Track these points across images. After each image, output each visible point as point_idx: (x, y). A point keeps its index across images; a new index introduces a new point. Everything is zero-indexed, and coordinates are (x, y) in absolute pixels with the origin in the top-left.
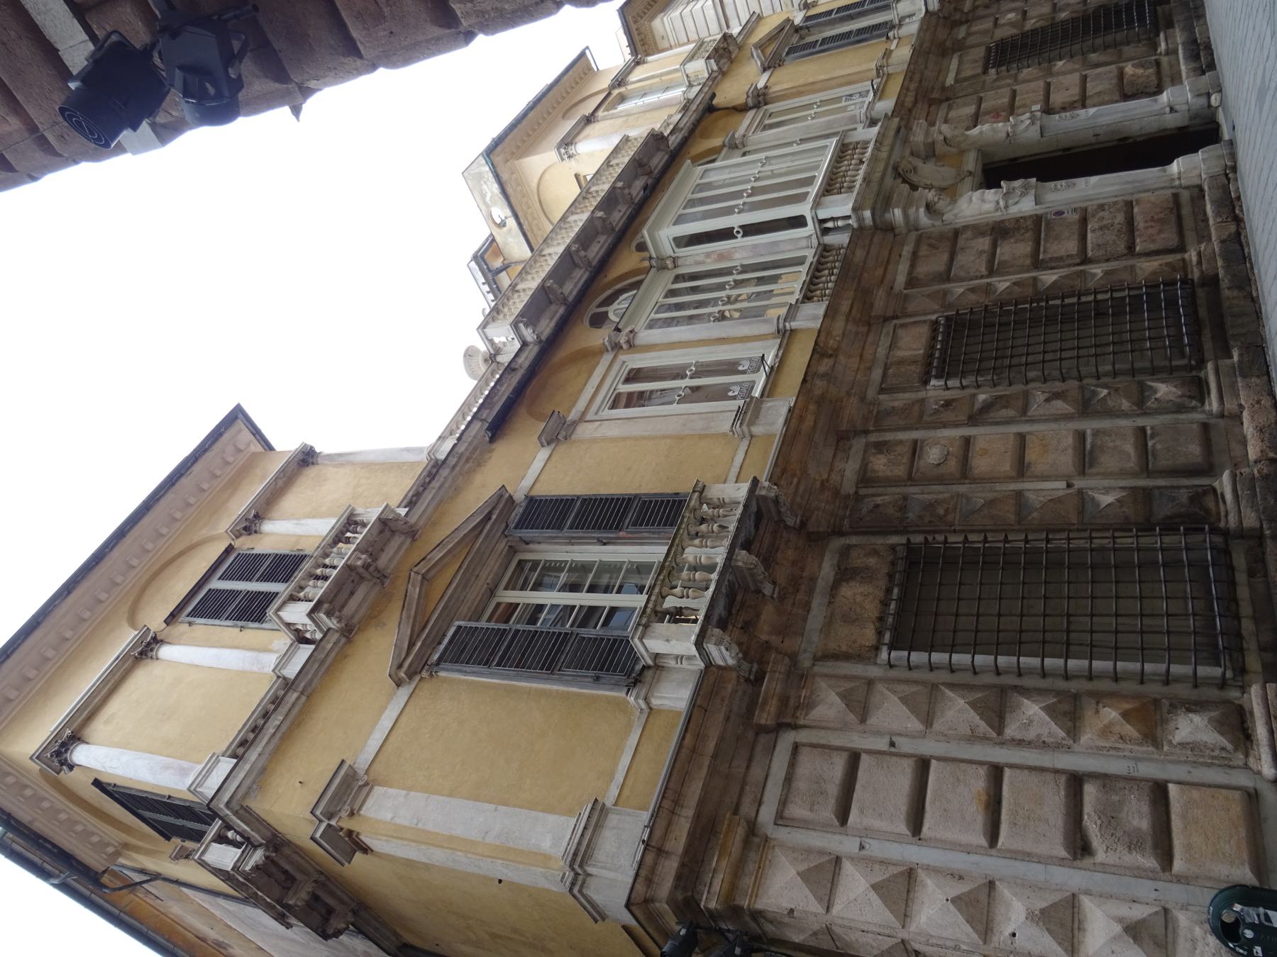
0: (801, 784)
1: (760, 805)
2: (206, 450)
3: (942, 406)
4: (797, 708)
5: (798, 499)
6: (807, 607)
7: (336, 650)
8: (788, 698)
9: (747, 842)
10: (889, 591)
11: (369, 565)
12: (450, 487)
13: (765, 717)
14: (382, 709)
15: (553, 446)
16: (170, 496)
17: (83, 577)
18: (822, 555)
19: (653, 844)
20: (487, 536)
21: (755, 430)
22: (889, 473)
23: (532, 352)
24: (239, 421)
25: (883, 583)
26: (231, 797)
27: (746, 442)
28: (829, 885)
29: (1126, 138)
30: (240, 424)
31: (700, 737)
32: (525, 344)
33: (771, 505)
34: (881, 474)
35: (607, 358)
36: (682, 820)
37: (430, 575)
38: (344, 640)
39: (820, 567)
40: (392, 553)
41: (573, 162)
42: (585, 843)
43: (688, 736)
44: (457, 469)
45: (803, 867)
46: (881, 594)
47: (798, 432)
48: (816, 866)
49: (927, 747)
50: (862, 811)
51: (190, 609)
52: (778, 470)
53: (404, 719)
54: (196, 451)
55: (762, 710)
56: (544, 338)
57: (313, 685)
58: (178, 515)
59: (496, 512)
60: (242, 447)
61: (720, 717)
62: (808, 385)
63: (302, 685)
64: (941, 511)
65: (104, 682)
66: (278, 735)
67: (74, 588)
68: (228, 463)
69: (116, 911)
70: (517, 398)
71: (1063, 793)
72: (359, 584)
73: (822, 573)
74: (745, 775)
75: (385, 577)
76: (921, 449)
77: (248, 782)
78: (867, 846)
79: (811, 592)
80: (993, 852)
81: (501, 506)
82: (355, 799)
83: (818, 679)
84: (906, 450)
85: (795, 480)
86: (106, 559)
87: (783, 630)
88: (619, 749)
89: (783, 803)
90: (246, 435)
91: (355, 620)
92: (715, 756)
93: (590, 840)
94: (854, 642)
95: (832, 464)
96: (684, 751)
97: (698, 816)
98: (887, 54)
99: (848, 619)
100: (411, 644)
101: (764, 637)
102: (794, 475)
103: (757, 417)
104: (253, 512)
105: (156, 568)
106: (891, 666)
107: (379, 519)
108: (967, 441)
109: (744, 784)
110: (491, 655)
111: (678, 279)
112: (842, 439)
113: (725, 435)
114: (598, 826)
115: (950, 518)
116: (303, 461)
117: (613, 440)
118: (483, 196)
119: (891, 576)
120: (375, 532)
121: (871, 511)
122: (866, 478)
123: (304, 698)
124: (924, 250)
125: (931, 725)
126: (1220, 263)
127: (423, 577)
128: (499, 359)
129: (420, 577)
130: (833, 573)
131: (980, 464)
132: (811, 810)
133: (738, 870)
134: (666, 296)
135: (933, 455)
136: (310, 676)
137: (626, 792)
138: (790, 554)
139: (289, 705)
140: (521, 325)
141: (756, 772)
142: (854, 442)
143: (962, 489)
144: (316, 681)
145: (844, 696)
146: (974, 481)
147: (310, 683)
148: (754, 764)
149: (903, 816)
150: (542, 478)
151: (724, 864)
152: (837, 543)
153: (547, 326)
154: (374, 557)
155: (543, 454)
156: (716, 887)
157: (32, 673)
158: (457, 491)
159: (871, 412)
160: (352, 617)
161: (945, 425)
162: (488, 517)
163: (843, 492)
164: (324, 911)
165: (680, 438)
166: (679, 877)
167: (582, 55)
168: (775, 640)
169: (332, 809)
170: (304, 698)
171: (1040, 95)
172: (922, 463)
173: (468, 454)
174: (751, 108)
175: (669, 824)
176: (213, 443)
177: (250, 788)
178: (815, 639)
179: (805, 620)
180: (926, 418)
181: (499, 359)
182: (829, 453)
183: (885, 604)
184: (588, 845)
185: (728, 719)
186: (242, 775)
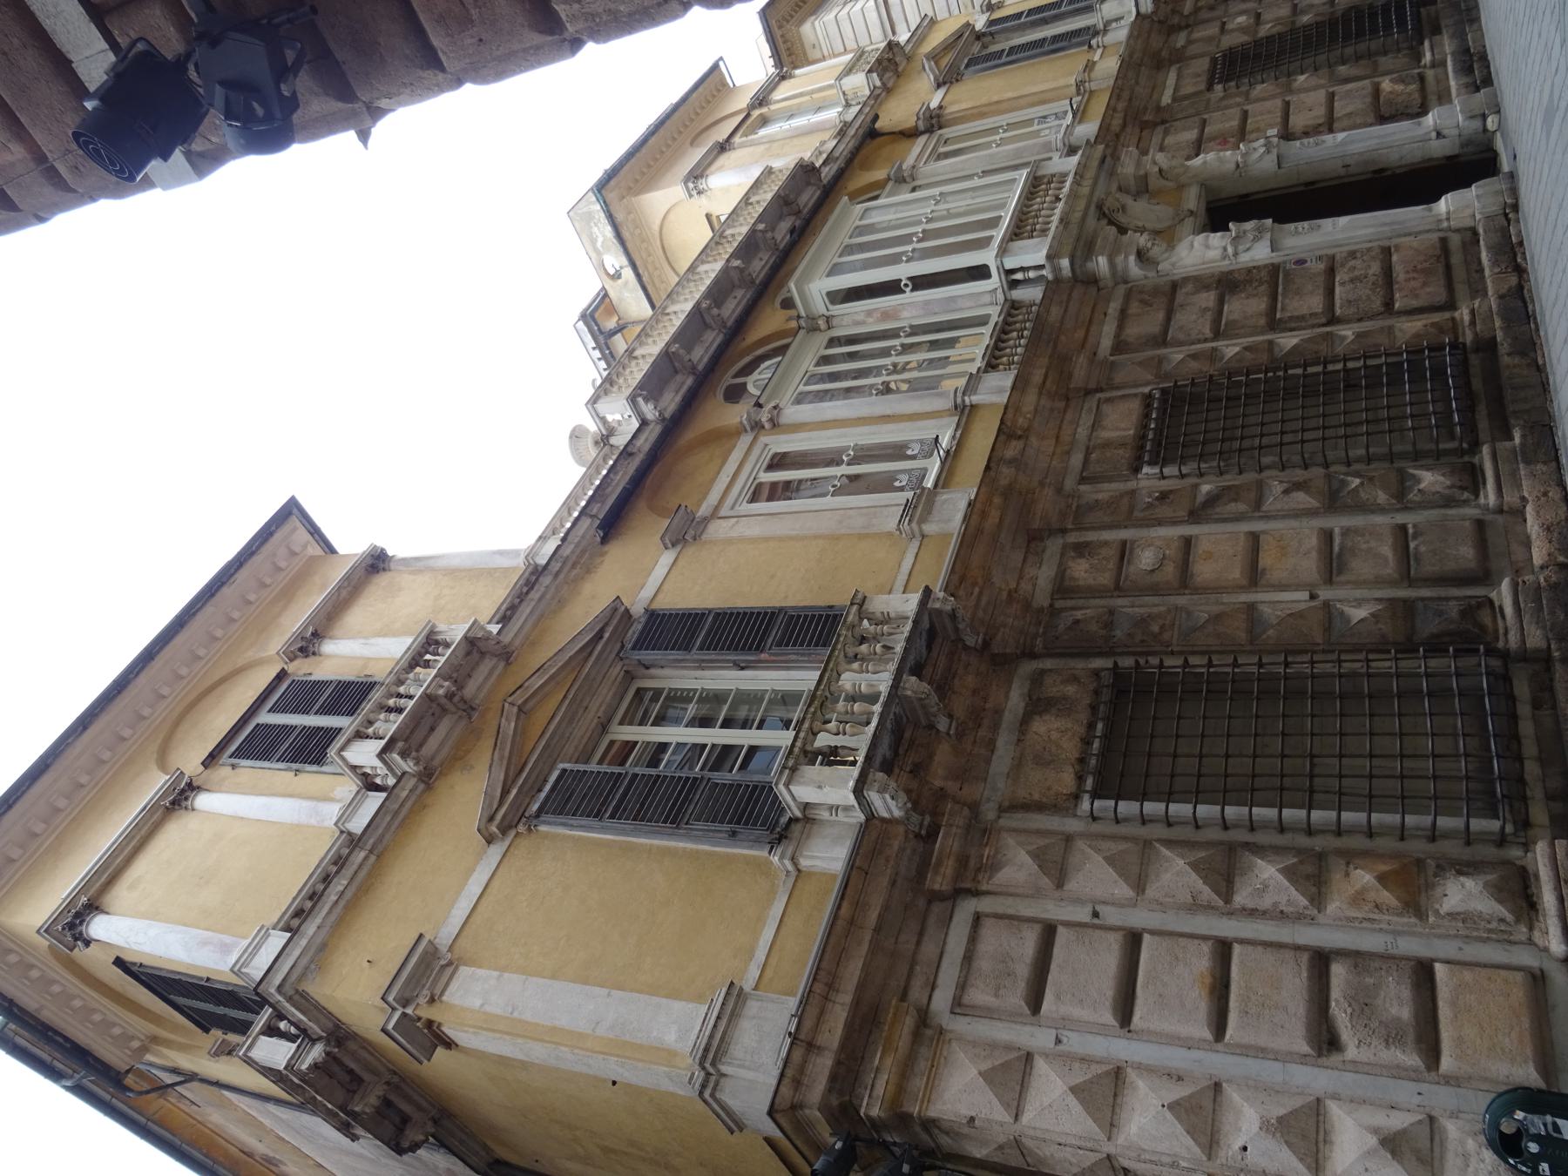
0: (983, 964)
1: (933, 989)
2: (253, 554)
3: (1157, 499)
4: (979, 870)
5: (980, 614)
6: (991, 745)
7: (413, 798)
8: (968, 857)
9: (917, 1035)
10: (1091, 726)
11: (453, 695)
12: (553, 598)
13: (940, 881)
14: (470, 872)
15: (679, 548)
16: (209, 609)
17: (102, 710)
18: (1010, 682)
19: (802, 1037)
20: (598, 659)
21: (927, 528)
22: (1091, 582)
23: (653, 432)
24: (294, 518)
25: (1084, 716)
26: (284, 980)
27: (916, 543)
28: (1018, 1088)
29: (1382, 170)
30: (294, 521)
31: (859, 906)
32: (644, 422)
33: (947, 621)
34: (1081, 583)
35: (745, 440)
36: (838, 1008)
37: (528, 707)
38: (422, 786)
39: (1007, 696)
40: (481, 679)
41: (703, 199)
42: (718, 1036)
43: (845, 904)
44: (562, 576)
45: (986, 1065)
46: (1082, 730)
47: (979, 531)
48: (1002, 1065)
49: (1138, 918)
50: (1058, 997)
51: (233, 748)
52: (956, 578)
53: (496, 883)
54: (240, 554)
55: (936, 873)
56: (667, 415)
57: (385, 842)
58: (219, 633)
59: (610, 630)
60: (297, 549)
61: (884, 881)
62: (992, 473)
63: (371, 841)
64: (1155, 628)
65: (128, 838)
66: (342, 903)
67: (91, 722)
68: (280, 569)
69: (143, 1120)
70: (634, 489)
71: (1305, 974)
72: (441, 718)
73: (1010, 704)
74: (915, 953)
75: (473, 709)
76: (1131, 552)
77: (304, 961)
78: (1065, 1040)
79: (995, 727)
80: (1219, 1046)
81: (615, 622)
82: (435, 981)
83: (1004, 835)
84: (1112, 553)
85: (977, 590)
86: (130, 687)
87: (962, 775)
88: (761, 920)
89: (962, 986)
90: (302, 535)
91: (436, 762)
92: (878, 930)
93: (725, 1033)
94: (1049, 789)
95: (1022, 570)
96: (840, 922)
97: (857, 1002)
98: (1090, 66)
99: (1042, 761)
100: (505, 792)
101: (938, 783)
102: (974, 584)
103: (930, 513)
104: (311, 629)
105: (191, 697)
106: (1094, 819)
107: (465, 637)
108: (1188, 542)
109: (913, 963)
110: (602, 805)
111: (832, 342)
112: (1033, 539)
113: (890, 534)
114: (735, 1016)
115: (1166, 636)
116: (372, 566)
117: (753, 540)
118: (593, 241)
119: (1094, 708)
120: (461, 654)
121: (1070, 628)
122: (1063, 588)
123: (373, 858)
124: (1134, 308)
125: (1143, 891)
126: (1498, 323)
127: (520, 709)
128: (613, 441)
129: (515, 709)
130: (1022, 705)
131: (1204, 571)
132: (996, 996)
133: (906, 1069)
134: (818, 364)
135: (1146, 559)
136: (380, 831)
137: (769, 973)
138: (970, 680)
139: (355, 867)
140: (640, 400)
141: (929, 949)
142: (1049, 543)
143: (1181, 601)
144: (387, 837)
145: (1037, 856)
146: (1196, 591)
147: (380, 839)
148: (926, 938)
149: (1108, 1003)
150: (665, 587)
151: (889, 1061)
152: (1028, 667)
153: (671, 401)
154: (459, 684)
155: (667, 558)
156: (880, 1090)
157: (39, 828)
158: (561, 603)
159: (1069, 506)
160: (433, 758)
161: (1160, 523)
162: (599, 636)
163: (1035, 605)
164: (397, 1120)
165: (835, 538)
166: (833, 1078)
167: (715, 68)
168: (952, 787)
169: (407, 995)
170: (373, 858)
171: (1277, 117)
172: (1132, 569)
173: (574, 558)
174: (922, 133)
175: (822, 1013)
176: (262, 544)
177: (307, 968)
178: (1001, 785)
179: (988, 761)
180: (1137, 514)
181: (613, 441)
182: (1018, 557)
183: (1087, 742)
184: (722, 1039)
185: (893, 883)
186: (297, 953)
